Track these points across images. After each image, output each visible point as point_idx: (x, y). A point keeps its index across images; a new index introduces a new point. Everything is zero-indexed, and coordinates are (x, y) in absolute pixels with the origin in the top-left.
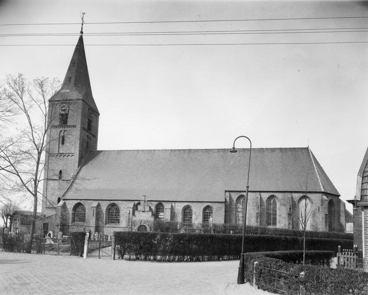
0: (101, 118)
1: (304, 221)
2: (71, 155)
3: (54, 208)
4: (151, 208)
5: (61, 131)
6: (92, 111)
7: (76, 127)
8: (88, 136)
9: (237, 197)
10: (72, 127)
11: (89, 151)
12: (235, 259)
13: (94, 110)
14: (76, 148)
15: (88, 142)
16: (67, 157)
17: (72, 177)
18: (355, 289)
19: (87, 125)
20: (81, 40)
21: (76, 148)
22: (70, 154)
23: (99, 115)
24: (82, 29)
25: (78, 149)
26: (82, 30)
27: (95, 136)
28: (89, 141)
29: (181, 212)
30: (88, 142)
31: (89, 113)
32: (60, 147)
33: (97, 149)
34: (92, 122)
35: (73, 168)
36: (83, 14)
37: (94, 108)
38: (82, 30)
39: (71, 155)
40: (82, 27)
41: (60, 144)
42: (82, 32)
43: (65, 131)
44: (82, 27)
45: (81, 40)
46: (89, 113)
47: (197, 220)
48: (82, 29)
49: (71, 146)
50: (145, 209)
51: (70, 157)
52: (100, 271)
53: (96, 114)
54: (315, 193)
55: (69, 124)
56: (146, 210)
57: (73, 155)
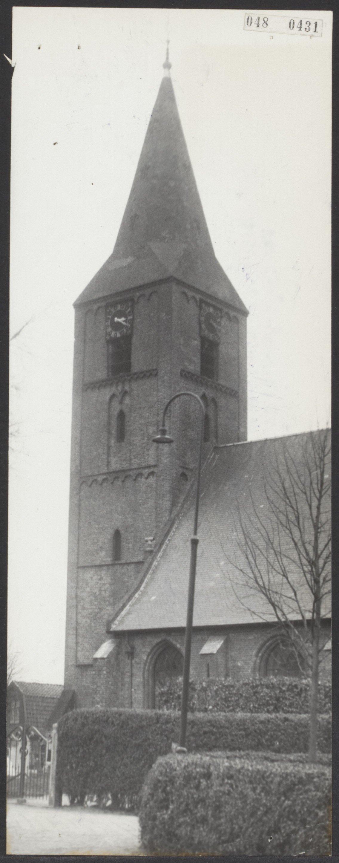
2: (146, 471)
5: (113, 396)
6: (215, 308)
7: (156, 375)
12: (117, 808)
15: (206, 418)
16: (135, 480)
18: (122, 795)
19: (197, 359)
23: (245, 313)
24: (168, 54)
26: (167, 58)
28: (211, 415)
30: (206, 418)
31: (202, 319)
32: (114, 449)
33: (246, 440)
37: (222, 293)
38: (167, 58)
39: (146, 471)
43: (125, 393)
44: (168, 50)
46: (202, 319)
48: (168, 54)
52: (306, 26)
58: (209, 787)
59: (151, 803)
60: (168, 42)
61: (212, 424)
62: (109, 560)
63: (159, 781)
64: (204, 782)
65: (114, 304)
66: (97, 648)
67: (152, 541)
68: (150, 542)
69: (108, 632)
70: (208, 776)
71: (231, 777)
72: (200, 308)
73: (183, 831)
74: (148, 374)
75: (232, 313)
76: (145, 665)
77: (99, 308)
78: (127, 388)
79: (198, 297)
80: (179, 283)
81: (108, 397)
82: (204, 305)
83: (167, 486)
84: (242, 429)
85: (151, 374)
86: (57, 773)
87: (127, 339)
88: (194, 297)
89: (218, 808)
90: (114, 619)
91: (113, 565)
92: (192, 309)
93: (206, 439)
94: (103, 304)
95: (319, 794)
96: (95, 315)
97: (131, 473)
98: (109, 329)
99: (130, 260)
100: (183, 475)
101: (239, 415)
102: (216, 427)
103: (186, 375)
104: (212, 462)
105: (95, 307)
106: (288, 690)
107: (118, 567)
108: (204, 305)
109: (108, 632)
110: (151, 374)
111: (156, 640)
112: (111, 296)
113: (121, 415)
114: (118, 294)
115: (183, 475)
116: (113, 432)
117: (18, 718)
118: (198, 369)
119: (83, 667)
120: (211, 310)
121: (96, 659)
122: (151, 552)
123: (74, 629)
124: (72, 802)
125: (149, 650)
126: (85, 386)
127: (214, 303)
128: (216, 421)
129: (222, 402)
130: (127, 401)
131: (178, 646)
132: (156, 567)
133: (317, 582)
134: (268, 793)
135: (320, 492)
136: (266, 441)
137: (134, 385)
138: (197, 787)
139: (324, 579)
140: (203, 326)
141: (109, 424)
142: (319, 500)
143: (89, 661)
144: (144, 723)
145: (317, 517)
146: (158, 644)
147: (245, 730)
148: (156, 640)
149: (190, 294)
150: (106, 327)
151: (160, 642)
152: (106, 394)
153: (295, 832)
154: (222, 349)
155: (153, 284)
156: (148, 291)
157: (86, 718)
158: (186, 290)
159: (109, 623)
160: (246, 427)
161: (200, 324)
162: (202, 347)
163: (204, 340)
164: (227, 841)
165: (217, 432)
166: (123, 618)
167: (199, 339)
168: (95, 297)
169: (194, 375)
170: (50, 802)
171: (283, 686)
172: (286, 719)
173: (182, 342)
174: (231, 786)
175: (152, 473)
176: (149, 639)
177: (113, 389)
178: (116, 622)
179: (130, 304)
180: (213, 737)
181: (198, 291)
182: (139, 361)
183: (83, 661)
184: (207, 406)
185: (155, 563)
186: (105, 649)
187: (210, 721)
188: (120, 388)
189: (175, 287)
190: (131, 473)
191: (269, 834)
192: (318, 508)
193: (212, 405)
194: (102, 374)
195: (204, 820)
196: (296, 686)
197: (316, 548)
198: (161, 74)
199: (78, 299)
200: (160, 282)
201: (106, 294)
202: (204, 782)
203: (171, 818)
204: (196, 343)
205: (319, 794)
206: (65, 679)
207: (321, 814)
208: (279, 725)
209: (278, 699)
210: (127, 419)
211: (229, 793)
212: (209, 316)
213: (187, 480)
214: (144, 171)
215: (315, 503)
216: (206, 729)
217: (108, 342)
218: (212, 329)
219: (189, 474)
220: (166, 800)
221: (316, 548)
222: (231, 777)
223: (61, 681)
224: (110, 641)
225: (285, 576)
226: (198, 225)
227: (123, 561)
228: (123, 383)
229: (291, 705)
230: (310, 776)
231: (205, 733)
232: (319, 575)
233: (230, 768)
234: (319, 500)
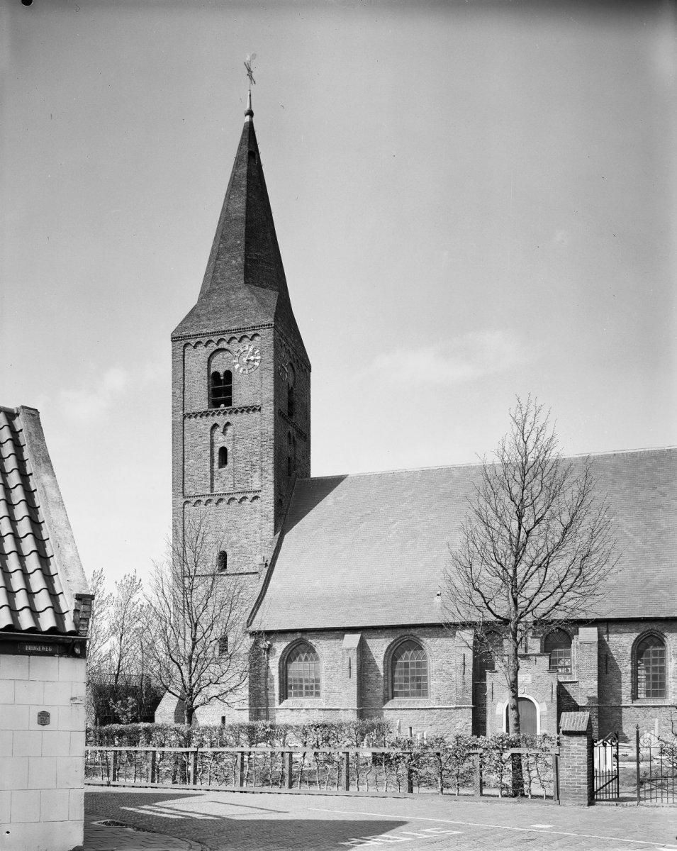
3: (509, 531)
7: (260, 410)
9: (385, 649)
10: (242, 412)
11: (296, 490)
14: (264, 474)
17: (262, 562)
20: (250, 132)
22: (248, 495)
25: (271, 478)
29: (630, 652)
35: (258, 535)
39: (250, 496)
41: (216, 465)
43: (228, 424)
45: (250, 132)
47: (108, 684)
49: (248, 468)
51: (247, 502)
54: (618, 624)
56: (529, 652)
57: (256, 498)
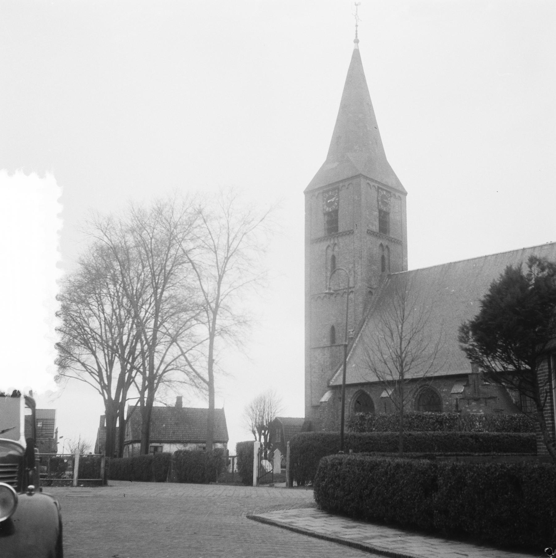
0: (409, 199)
1: (371, 352)
4: (212, 357)
5: (329, 246)
6: (386, 191)
8: (381, 245)
13: (391, 188)
19: (377, 223)
21: (356, 276)
23: (405, 194)
24: (356, 34)
26: (357, 37)
27: (400, 243)
28: (386, 256)
30: (383, 258)
31: (379, 198)
33: (407, 270)
34: (388, 214)
36: (356, 5)
38: (357, 37)
40: (357, 31)
42: (357, 41)
43: (335, 244)
44: (357, 31)
45: (356, 58)
48: (356, 34)
50: (179, 356)
53: (397, 194)
55: (341, 230)
58: (341, 469)
59: (318, 479)
60: (357, 26)
61: (387, 261)
62: (328, 344)
63: (322, 468)
64: (339, 467)
65: (327, 192)
66: (322, 395)
67: (352, 332)
68: (351, 333)
69: (329, 386)
70: (340, 464)
71: (349, 464)
72: (378, 192)
73: (331, 491)
74: (348, 233)
75: (397, 194)
76: (350, 405)
77: (318, 194)
78: (336, 242)
79: (376, 185)
80: (366, 178)
81: (325, 248)
82: (380, 190)
83: (360, 299)
84: (404, 263)
85: (350, 233)
86: (290, 469)
87: (336, 212)
88: (374, 186)
89: (344, 479)
90: (331, 379)
91: (331, 346)
92: (374, 194)
93: (383, 270)
94: (321, 191)
95: (383, 470)
96: (317, 198)
97: (339, 292)
98: (325, 206)
99: (336, 164)
100: (370, 292)
101: (403, 255)
102: (389, 263)
103: (371, 233)
104: (387, 283)
105: (316, 193)
106: (416, 418)
107: (334, 348)
108: (380, 190)
109: (329, 386)
110: (350, 233)
111: (356, 390)
112: (326, 186)
113: (334, 258)
114: (329, 185)
115: (370, 292)
116: (329, 268)
117: (280, 439)
118: (378, 229)
119: (315, 407)
120: (385, 193)
121: (321, 403)
122: (352, 338)
123: (310, 386)
124: (298, 484)
125: (352, 396)
126: (312, 241)
127: (386, 189)
128: (389, 260)
129: (392, 248)
130: (336, 249)
131: (368, 393)
132: (355, 347)
133: (401, 365)
134: (363, 470)
135: (403, 320)
136: (418, 270)
137: (340, 240)
138: (336, 469)
139: (406, 364)
140: (380, 203)
141: (326, 263)
142: (402, 325)
143: (319, 404)
144: (334, 439)
145: (401, 333)
146: (356, 392)
147: (388, 441)
148: (356, 390)
149: (372, 184)
150: (323, 206)
151: (358, 391)
152: (324, 245)
153: (374, 488)
154: (391, 216)
155: (348, 179)
156: (347, 184)
157: (305, 437)
158: (369, 182)
159: (329, 381)
160: (407, 262)
161: (378, 201)
162: (380, 215)
163: (380, 211)
164: (347, 495)
165: (389, 266)
166: (336, 378)
167: (377, 210)
168: (316, 187)
169: (375, 232)
170: (287, 485)
171: (413, 416)
172: (410, 435)
173: (368, 213)
174: (349, 468)
175: (352, 292)
176: (351, 389)
177: (328, 243)
178: (333, 380)
179: (337, 191)
180: (371, 446)
181: (376, 182)
182: (342, 226)
183: (315, 403)
184: (383, 250)
185: (354, 345)
186: (327, 397)
187: (369, 437)
188: (332, 242)
189: (363, 182)
190: (339, 292)
191: (364, 490)
192: (402, 328)
193: (386, 250)
194: (321, 233)
195: (339, 485)
196: (420, 416)
197: (401, 348)
198: (352, 46)
199: (307, 188)
200: (353, 178)
201: (322, 185)
202: (339, 467)
203: (326, 486)
204: (376, 213)
205: (383, 470)
206: (306, 414)
207: (383, 479)
208: (406, 438)
209: (410, 424)
210: (336, 260)
211: (349, 471)
212: (383, 196)
213: (372, 294)
214: (344, 107)
215: (400, 326)
216: (367, 441)
217: (325, 214)
218: (386, 204)
219: (373, 291)
220: (324, 476)
221: (401, 348)
222: (349, 464)
223: (304, 417)
224: (329, 391)
225: (386, 364)
226: (377, 141)
227: (336, 344)
228: (334, 238)
229: (417, 426)
230: (380, 462)
231: (367, 443)
232: (402, 362)
233: (349, 460)
234: (402, 325)
